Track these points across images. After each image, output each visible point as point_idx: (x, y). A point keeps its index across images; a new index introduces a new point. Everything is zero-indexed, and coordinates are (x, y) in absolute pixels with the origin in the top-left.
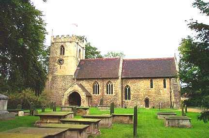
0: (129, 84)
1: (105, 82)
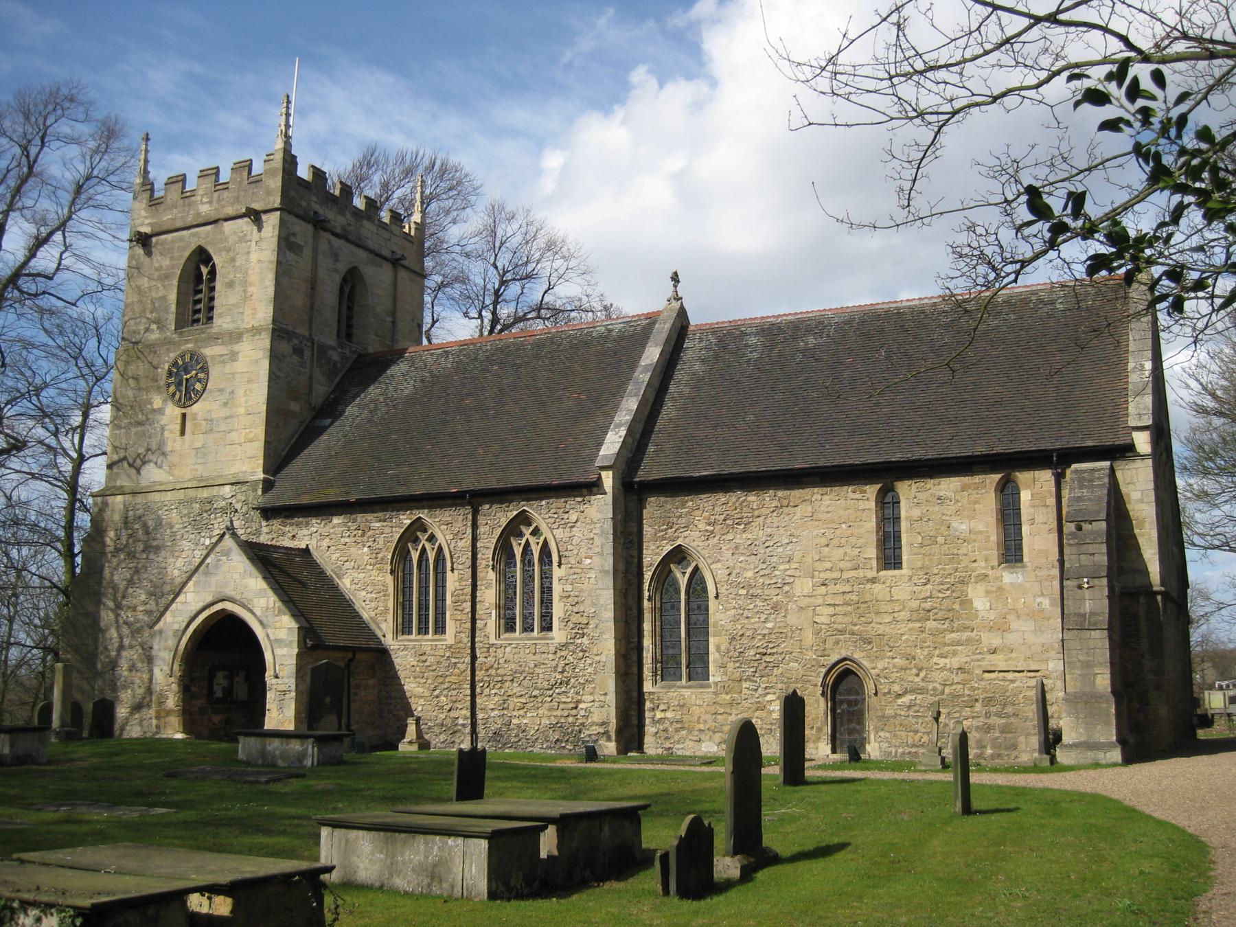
0: (691, 539)
1: (497, 518)
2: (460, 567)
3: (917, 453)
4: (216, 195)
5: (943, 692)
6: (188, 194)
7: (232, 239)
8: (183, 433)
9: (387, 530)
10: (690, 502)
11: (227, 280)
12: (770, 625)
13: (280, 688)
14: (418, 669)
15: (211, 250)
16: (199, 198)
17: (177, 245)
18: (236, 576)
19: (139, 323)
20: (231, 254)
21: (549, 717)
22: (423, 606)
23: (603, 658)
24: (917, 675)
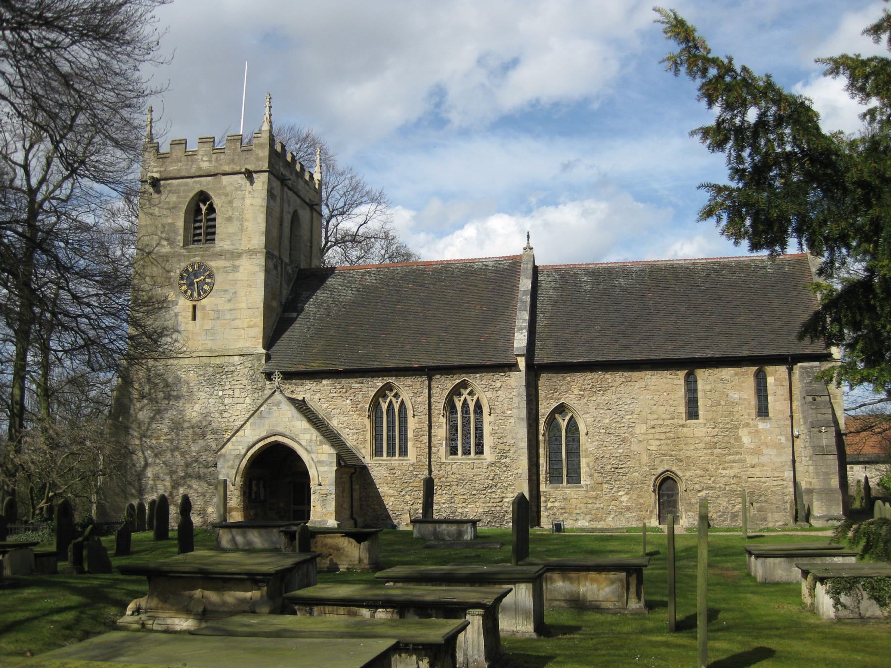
0: (570, 399)
1: (445, 385)
2: (419, 414)
3: (710, 354)
4: (214, 156)
5: (725, 489)
6: (190, 153)
7: (229, 189)
8: (194, 318)
9: (365, 389)
10: (569, 377)
11: (226, 216)
12: (620, 451)
13: (323, 492)
14: (389, 478)
15: (211, 194)
16: (200, 157)
17: (182, 188)
18: (286, 420)
19: (152, 239)
20: (229, 198)
21: (483, 507)
22: (391, 439)
23: (520, 471)
24: (710, 480)
